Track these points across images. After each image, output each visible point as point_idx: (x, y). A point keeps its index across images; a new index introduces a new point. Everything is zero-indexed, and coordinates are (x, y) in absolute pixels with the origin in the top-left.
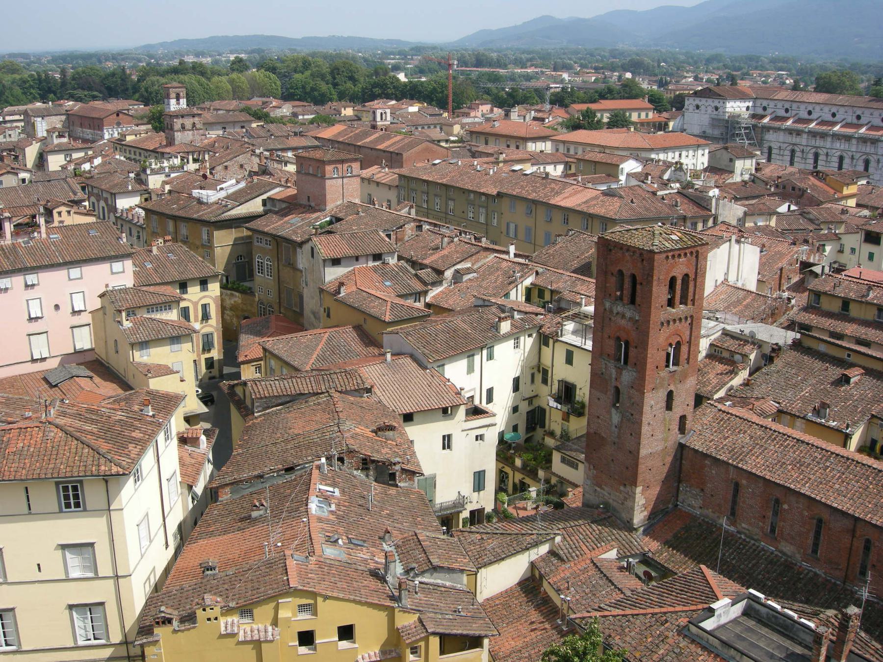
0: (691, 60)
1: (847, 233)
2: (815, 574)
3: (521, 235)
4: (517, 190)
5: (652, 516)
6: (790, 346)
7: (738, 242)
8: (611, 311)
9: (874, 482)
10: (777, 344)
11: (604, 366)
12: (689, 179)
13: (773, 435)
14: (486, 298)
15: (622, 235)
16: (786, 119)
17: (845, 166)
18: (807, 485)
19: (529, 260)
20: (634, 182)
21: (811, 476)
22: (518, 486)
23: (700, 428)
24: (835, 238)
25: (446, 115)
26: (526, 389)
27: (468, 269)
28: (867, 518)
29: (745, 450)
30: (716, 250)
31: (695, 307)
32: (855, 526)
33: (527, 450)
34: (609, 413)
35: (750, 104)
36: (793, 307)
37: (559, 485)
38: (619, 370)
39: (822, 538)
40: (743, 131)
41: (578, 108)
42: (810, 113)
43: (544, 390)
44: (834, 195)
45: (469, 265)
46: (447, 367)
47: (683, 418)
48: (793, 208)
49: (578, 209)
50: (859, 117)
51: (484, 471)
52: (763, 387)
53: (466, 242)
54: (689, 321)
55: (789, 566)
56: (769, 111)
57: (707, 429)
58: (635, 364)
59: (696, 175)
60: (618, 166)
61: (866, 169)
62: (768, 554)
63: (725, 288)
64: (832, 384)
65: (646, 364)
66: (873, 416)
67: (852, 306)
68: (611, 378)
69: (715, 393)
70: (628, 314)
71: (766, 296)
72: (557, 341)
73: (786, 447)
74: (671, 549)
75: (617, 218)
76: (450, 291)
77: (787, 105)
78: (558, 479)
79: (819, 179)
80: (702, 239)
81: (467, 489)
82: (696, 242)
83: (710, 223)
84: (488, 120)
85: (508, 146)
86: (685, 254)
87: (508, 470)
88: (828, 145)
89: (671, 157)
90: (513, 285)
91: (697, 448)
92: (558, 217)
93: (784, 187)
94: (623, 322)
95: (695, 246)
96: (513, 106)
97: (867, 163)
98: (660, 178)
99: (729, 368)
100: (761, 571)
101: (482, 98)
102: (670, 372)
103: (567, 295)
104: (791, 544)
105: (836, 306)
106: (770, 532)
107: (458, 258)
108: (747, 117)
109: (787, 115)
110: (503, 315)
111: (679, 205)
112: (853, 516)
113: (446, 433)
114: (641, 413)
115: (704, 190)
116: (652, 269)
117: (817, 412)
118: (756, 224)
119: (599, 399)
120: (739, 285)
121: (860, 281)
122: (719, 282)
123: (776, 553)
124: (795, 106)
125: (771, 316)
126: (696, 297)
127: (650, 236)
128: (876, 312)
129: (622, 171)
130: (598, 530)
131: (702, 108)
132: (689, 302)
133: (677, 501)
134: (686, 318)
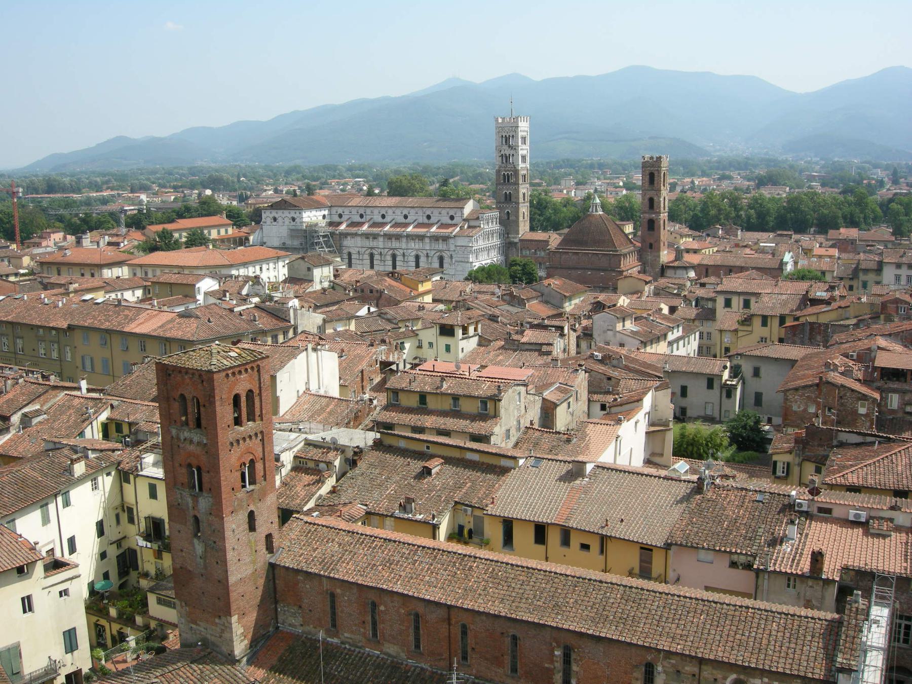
0: (270, 173)
1: (425, 328)
2: (422, 669)
3: (99, 367)
4: (89, 321)
5: (253, 643)
6: (371, 446)
7: (315, 350)
8: (178, 438)
9: (461, 567)
10: (358, 447)
12: (267, 291)
13: (360, 538)
14: (56, 440)
15: (179, 358)
16: (361, 224)
17: (421, 264)
18: (399, 583)
19: (104, 394)
20: (212, 300)
21: (402, 573)
22: (117, 638)
24: (412, 334)
25: (14, 246)
26: (112, 533)
27: (37, 411)
28: (459, 604)
30: (293, 361)
31: (264, 422)
32: (449, 615)
33: (121, 597)
35: (326, 212)
36: (375, 407)
37: (159, 629)
38: (195, 498)
39: (421, 632)
40: (321, 240)
41: (155, 229)
42: (383, 216)
43: (132, 530)
44: (410, 293)
45: (38, 407)
46: (17, 522)
47: (269, 537)
48: (373, 309)
49: (154, 334)
50: (429, 217)
51: (75, 629)
52: (349, 491)
53: (32, 383)
54: (260, 437)
55: (395, 666)
56: (345, 217)
57: (295, 544)
58: (210, 489)
59: (274, 287)
60: (194, 285)
61: (441, 265)
62: (374, 659)
63: (308, 397)
64: (415, 478)
66: (456, 503)
67: (429, 399)
68: (188, 508)
69: (304, 505)
70: (196, 439)
71: (348, 401)
72: (138, 475)
73: (375, 548)
74: (277, 674)
75: (195, 339)
76: (19, 438)
77: (361, 211)
78: (156, 622)
79: (396, 279)
80: (262, 353)
81: (57, 651)
82: (255, 356)
83: (291, 334)
84: (61, 249)
85: (83, 275)
86: (246, 370)
87: (103, 622)
88: (404, 246)
89: (251, 271)
90: (87, 422)
91: (287, 565)
92: (134, 346)
93: (362, 291)
94: (192, 448)
95: (255, 361)
96: (84, 232)
97: (441, 259)
98: (239, 293)
99: (315, 478)
100: (370, 678)
101: (54, 226)
102: (248, 492)
103: (143, 425)
104: (394, 644)
105: (414, 402)
107: (24, 401)
108: (324, 225)
109: (363, 220)
110: (75, 457)
111: (257, 319)
112: (446, 605)
113: (25, 595)
114: (223, 539)
115: (283, 302)
116: (213, 389)
117: (403, 508)
118: (335, 330)
120: (322, 392)
121: (434, 374)
122: (301, 393)
123: (382, 656)
124: (368, 211)
125: (354, 420)
126: (264, 412)
127: (207, 356)
128: (451, 401)
129: (199, 291)
130: (200, 669)
131: (280, 220)
132: (257, 418)
134: (256, 434)
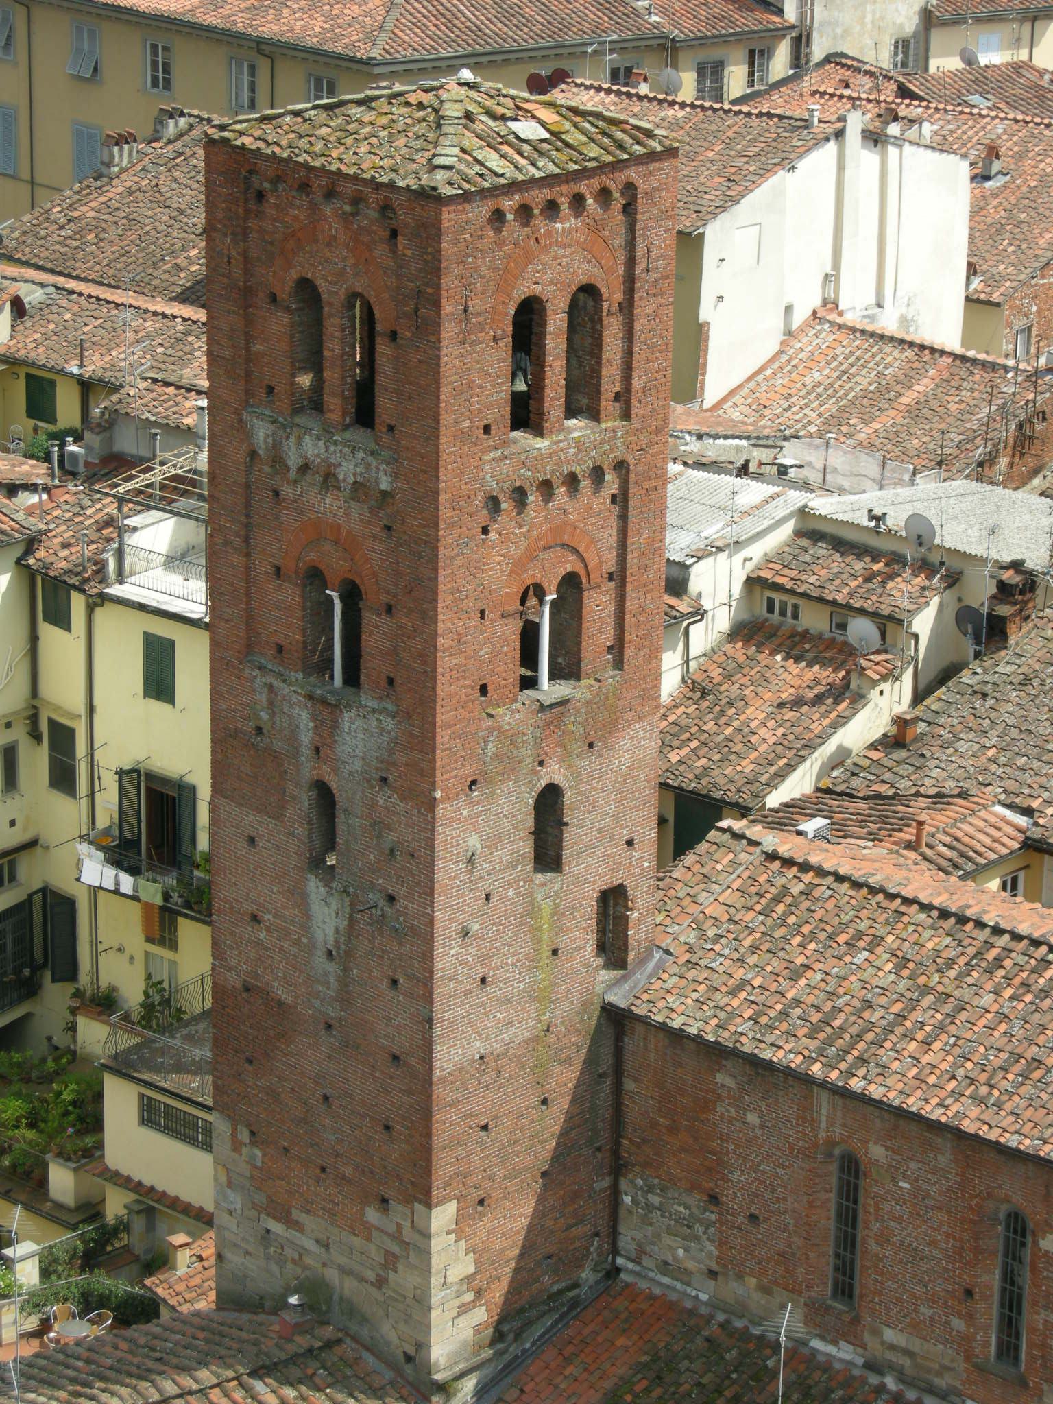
7: (874, 138)
8: (278, 460)
10: (1017, 565)
11: (263, 698)
13: (989, 945)
23: (691, 937)
29: (875, 1016)
30: (780, 178)
31: (636, 423)
34: (303, 901)
37: (138, 1224)
52: (962, 746)
54: (612, 483)
58: (391, 681)
65: (430, 676)
69: (772, 785)
71: (994, 367)
72: (103, 599)
75: (376, 53)
78: (130, 1197)
80: (649, 134)
82: (621, 146)
83: (780, 63)
86: (578, 201)
91: (676, 1023)
94: (330, 505)
95: (617, 165)
99: (827, 676)
102: (543, 708)
106: (1000, 1355)
116: (433, 269)
118: (970, 61)
119: (252, 840)
120: (888, 323)
122: (801, 316)
127: (420, 129)
132: (607, 404)
133: (615, 1251)
134: (597, 474)
